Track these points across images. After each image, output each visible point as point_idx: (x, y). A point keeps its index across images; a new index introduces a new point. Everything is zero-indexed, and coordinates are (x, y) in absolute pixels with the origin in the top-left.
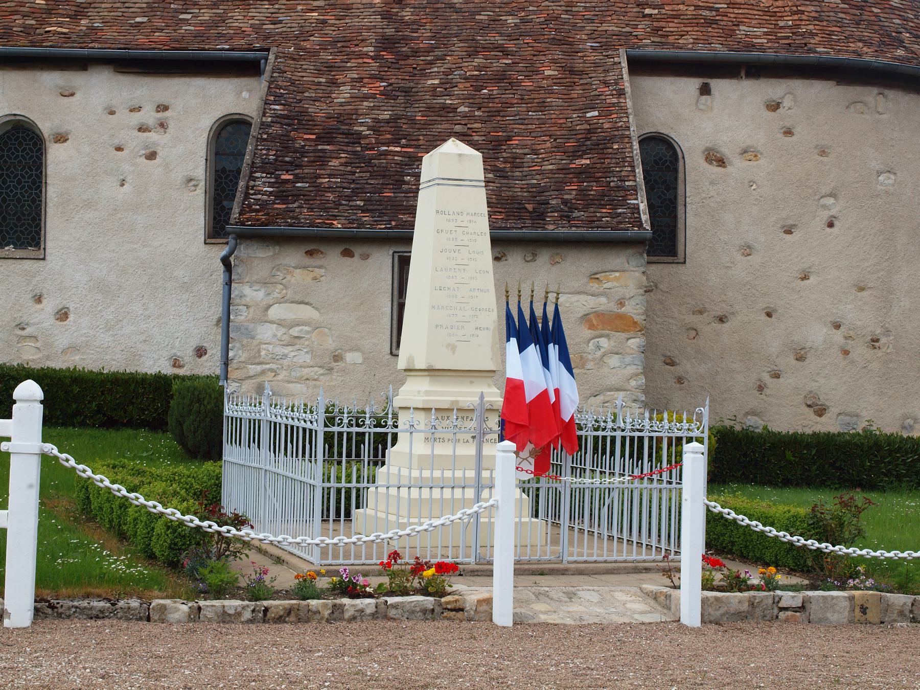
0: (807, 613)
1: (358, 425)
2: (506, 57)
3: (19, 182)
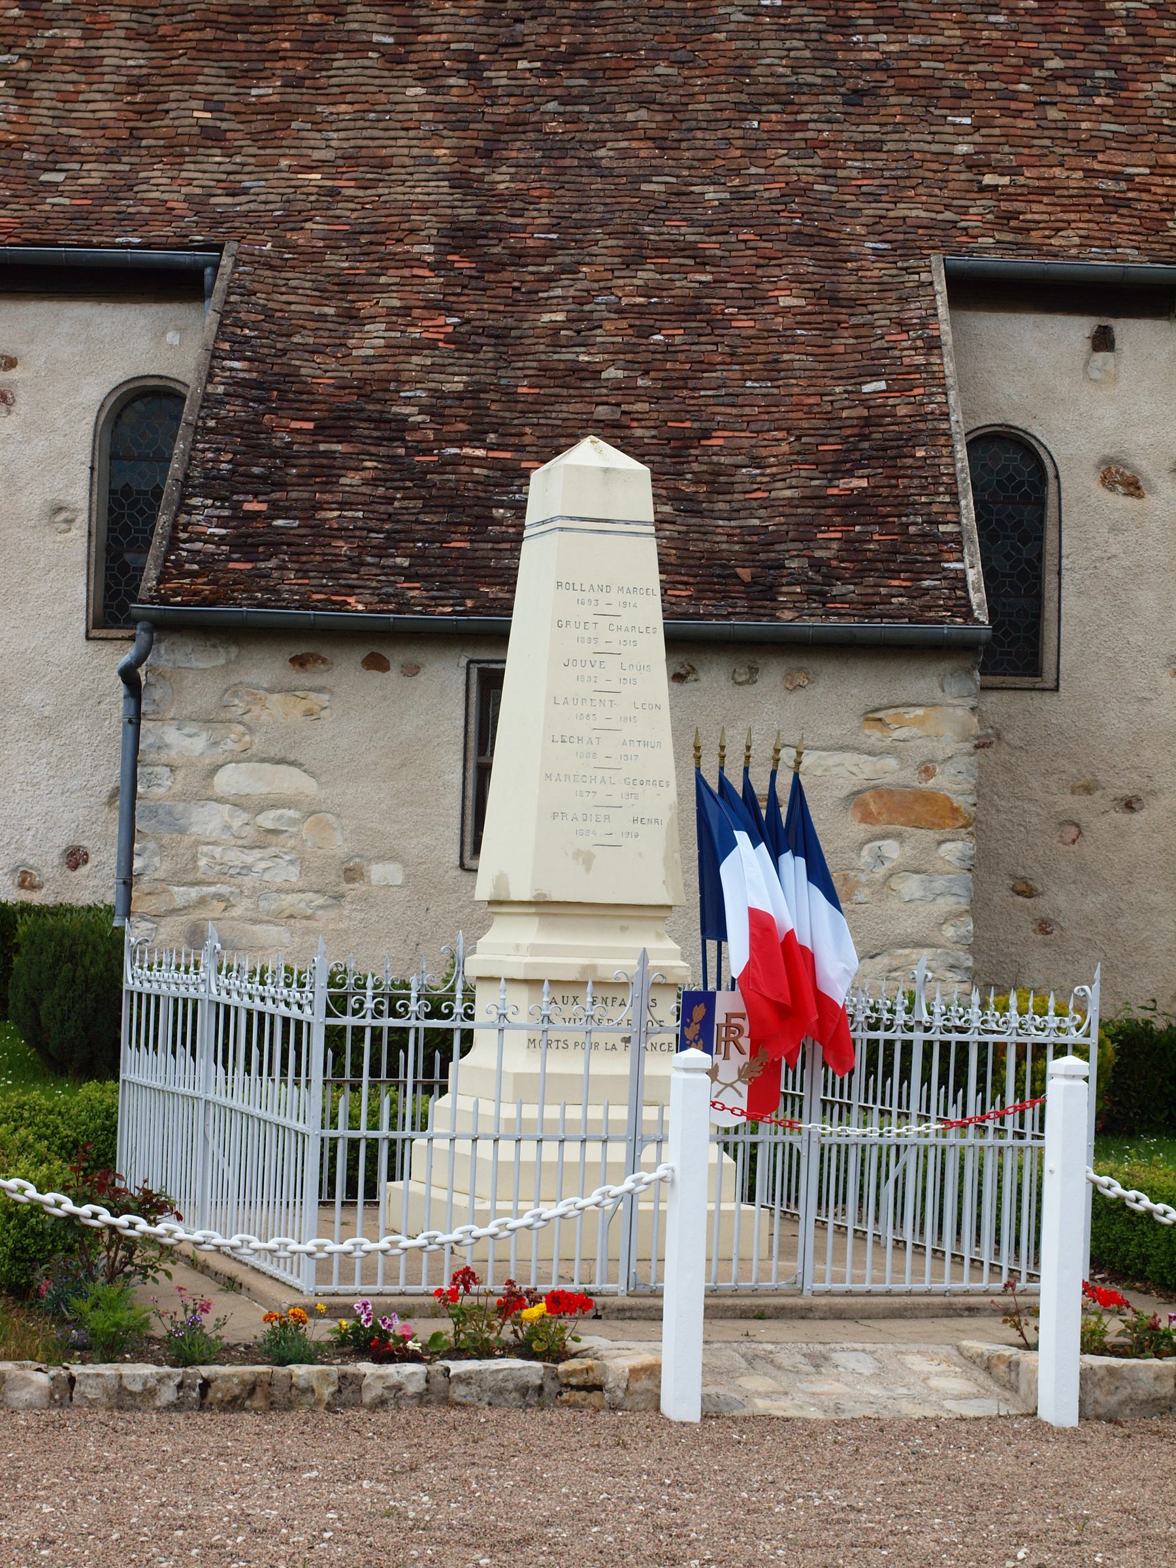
1: (393, 1013)
2: (701, 268)
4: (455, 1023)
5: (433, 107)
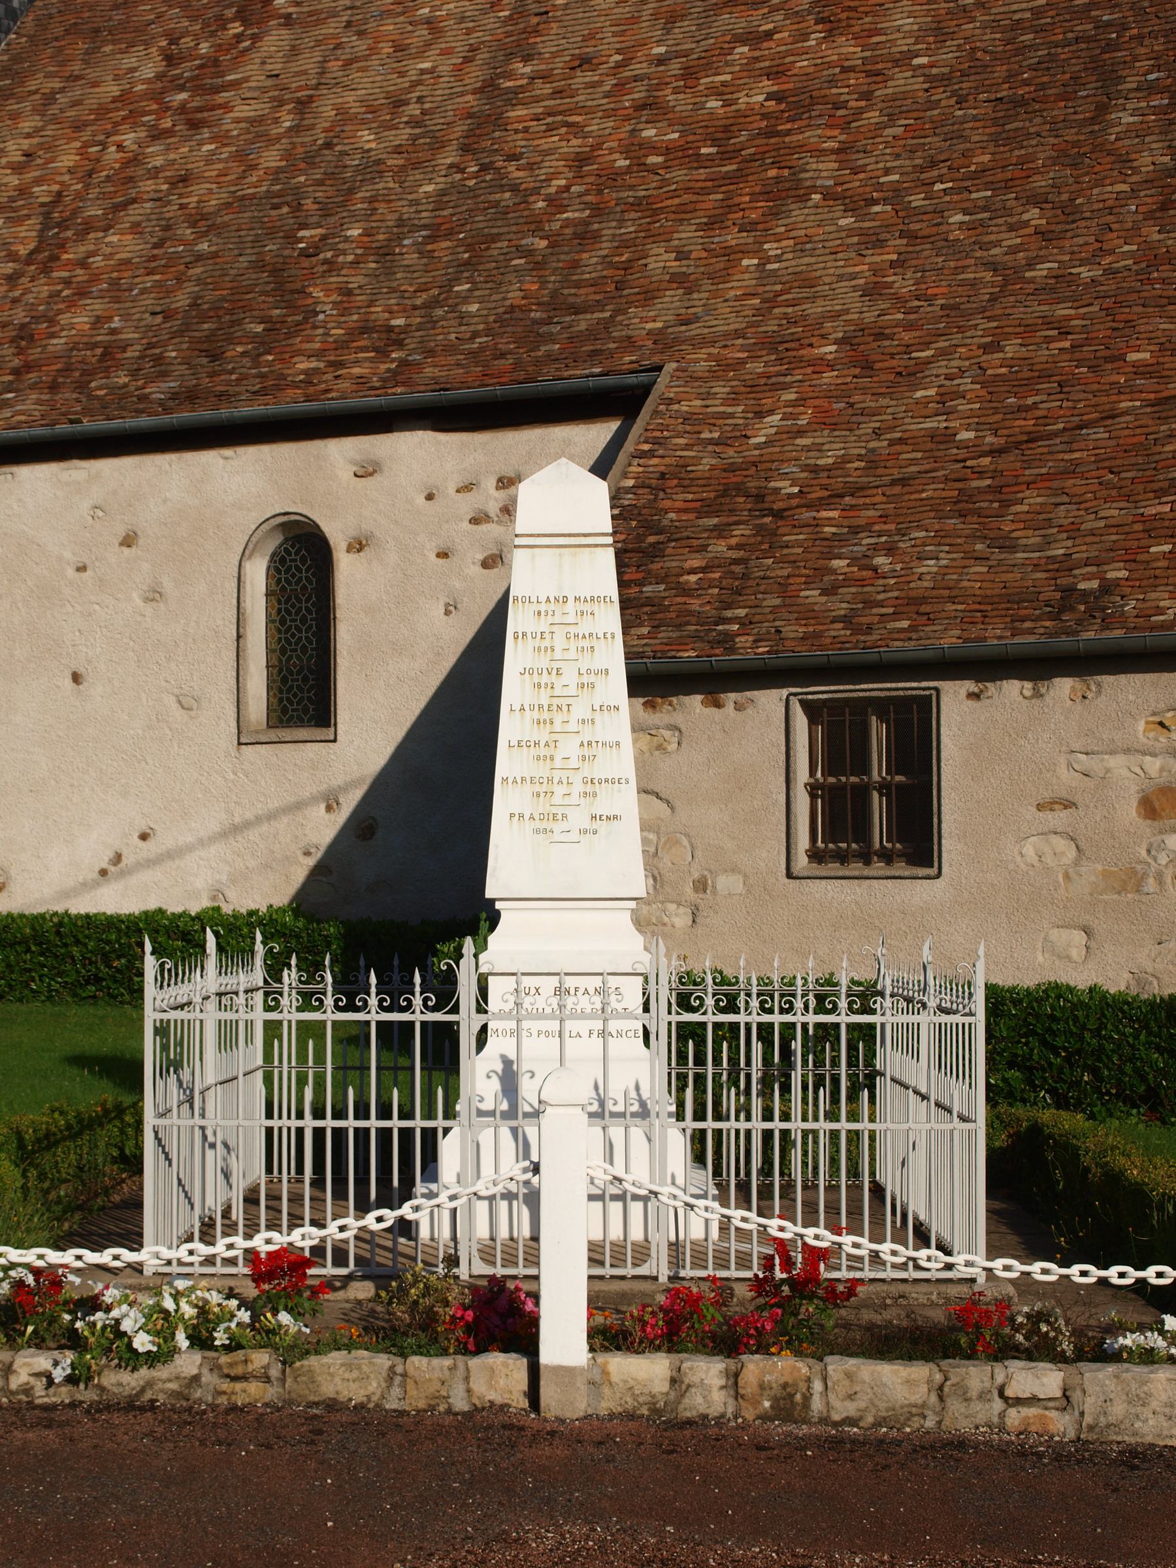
0: (1077, 1413)
1: (820, 1009)
2: (1064, 336)
3: (304, 620)
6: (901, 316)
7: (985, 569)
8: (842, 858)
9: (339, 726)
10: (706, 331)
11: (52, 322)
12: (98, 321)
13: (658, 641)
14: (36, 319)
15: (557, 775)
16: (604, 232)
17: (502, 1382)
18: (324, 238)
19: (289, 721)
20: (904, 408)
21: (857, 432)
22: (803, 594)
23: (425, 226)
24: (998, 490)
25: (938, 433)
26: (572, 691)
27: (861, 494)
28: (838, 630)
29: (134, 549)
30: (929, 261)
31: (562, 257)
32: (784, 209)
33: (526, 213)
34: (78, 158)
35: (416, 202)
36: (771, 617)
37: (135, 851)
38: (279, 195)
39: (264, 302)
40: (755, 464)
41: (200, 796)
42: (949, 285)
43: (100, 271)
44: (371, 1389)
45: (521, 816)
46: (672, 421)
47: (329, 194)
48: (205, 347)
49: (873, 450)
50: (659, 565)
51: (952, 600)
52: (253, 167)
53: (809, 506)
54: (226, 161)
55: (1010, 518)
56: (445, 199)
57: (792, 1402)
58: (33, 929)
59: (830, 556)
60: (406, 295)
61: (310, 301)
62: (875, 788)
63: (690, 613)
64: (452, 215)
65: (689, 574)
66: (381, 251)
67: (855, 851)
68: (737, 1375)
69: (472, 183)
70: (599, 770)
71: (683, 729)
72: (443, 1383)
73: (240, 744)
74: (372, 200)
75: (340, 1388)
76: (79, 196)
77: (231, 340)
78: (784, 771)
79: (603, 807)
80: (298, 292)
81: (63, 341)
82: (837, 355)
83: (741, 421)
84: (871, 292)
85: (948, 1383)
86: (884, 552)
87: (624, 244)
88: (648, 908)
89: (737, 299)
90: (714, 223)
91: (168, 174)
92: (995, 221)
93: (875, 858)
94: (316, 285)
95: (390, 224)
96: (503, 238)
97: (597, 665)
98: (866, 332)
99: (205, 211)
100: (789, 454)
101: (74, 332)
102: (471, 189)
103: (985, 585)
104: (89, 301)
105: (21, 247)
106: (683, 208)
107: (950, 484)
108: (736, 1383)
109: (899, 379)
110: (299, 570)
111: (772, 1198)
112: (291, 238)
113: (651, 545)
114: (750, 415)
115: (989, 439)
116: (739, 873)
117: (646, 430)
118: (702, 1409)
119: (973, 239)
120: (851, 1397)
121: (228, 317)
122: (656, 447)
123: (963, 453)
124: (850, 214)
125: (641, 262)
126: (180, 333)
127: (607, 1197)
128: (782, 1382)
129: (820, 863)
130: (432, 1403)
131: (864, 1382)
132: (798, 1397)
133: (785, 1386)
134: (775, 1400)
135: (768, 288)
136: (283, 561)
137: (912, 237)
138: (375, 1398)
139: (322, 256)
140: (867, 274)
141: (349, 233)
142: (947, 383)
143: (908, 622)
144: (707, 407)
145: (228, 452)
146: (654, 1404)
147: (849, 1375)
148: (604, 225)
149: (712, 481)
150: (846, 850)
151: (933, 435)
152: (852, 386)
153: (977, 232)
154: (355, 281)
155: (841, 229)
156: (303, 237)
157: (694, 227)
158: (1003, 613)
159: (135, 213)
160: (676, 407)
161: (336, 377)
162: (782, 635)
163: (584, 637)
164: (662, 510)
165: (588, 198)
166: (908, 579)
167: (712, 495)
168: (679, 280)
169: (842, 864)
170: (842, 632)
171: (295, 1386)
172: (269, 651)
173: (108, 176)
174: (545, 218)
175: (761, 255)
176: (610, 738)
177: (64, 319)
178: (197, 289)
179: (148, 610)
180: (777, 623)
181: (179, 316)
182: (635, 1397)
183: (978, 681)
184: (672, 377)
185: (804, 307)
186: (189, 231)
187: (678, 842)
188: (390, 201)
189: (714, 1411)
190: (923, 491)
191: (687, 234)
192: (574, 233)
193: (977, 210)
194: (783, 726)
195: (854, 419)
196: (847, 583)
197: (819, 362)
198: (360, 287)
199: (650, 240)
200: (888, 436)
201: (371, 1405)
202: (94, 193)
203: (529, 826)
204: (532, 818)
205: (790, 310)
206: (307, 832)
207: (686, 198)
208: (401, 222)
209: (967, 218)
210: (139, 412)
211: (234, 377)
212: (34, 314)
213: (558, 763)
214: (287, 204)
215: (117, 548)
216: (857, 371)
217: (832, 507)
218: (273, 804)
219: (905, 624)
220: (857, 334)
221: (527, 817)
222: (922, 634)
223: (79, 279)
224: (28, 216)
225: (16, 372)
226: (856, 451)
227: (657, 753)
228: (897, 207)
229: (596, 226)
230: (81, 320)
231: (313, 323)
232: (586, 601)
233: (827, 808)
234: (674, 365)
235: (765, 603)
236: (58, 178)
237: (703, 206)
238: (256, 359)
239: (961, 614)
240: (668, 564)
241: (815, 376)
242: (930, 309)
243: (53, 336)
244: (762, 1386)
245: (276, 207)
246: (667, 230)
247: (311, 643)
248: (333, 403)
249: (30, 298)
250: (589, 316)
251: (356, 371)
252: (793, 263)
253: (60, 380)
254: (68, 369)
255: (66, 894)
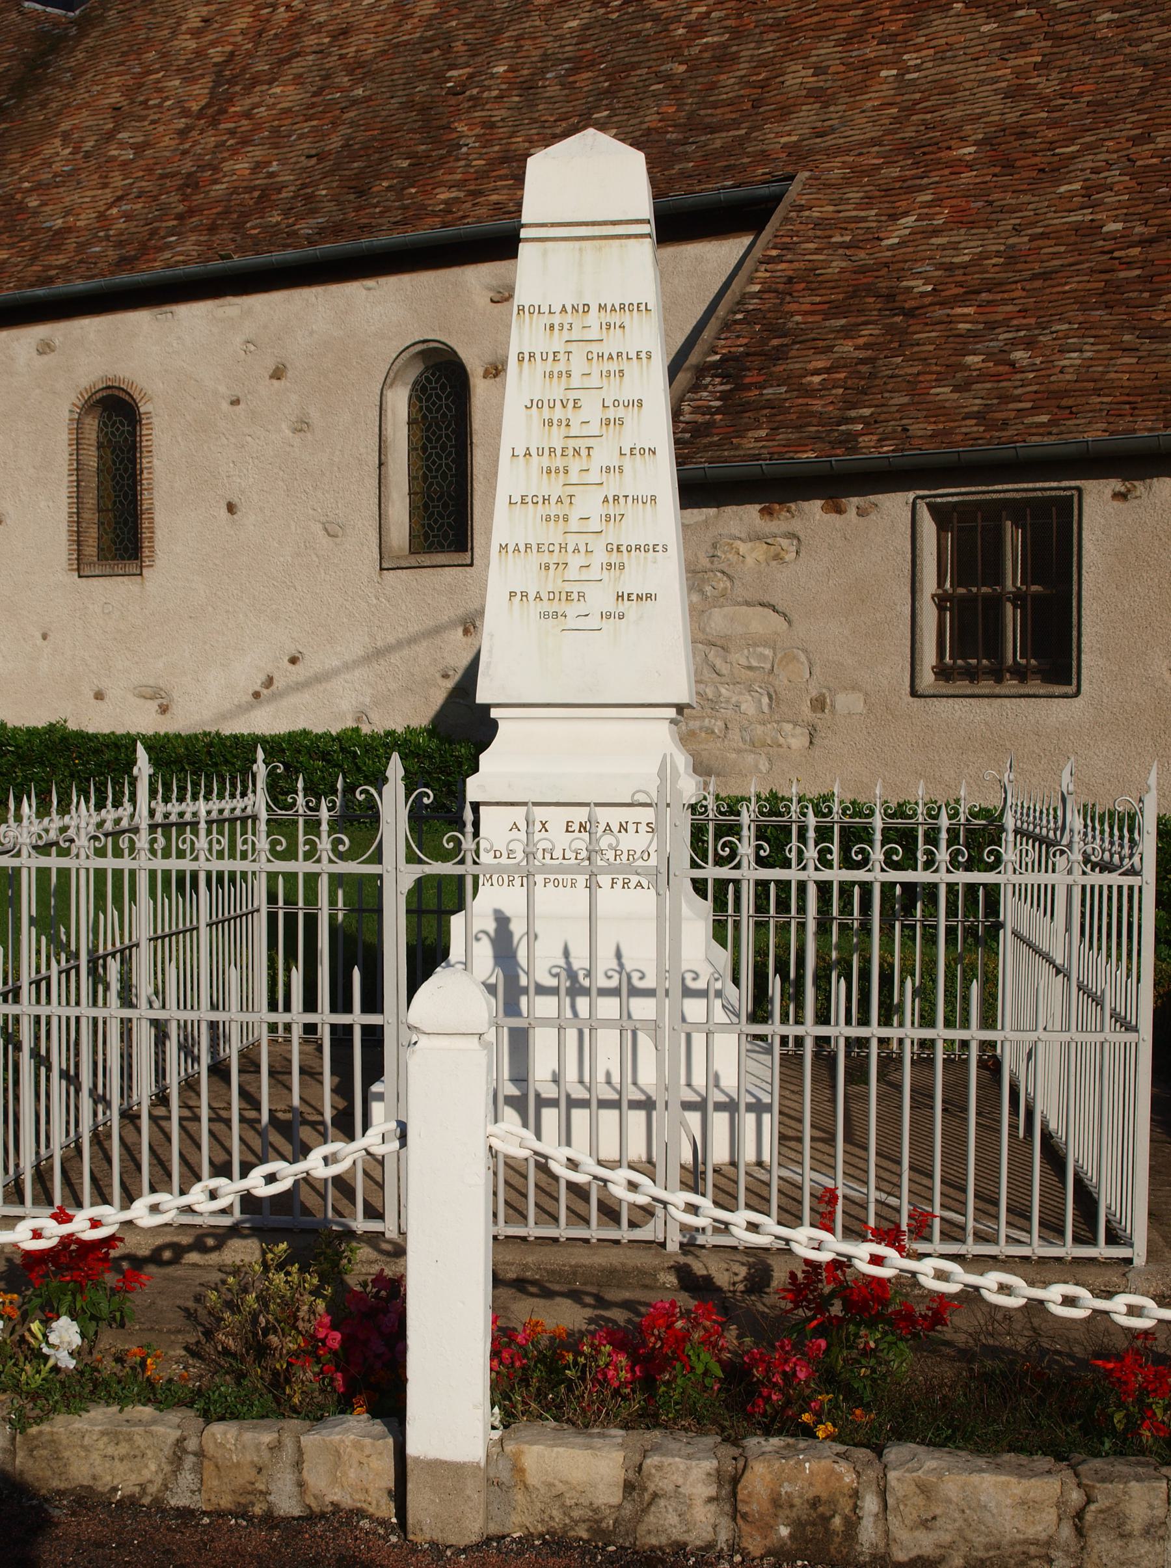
3: (443, 448)
4: (468, 869)
5: (1002, 37)
6: (1045, 115)
7: (1134, 360)
8: (972, 675)
9: (475, 550)
10: (842, 141)
11: (216, 169)
12: (258, 166)
13: (776, 443)
14: (201, 168)
15: (572, 541)
16: (742, 54)
17: (352, 1474)
18: (471, 76)
19: (430, 547)
20: (1046, 203)
21: (995, 230)
22: (933, 391)
23: (567, 59)
24: (1150, 279)
25: (1083, 226)
26: (594, 429)
27: (999, 289)
28: (971, 427)
29: (283, 382)
30: (1075, 60)
31: (700, 80)
32: (924, 19)
33: (666, 41)
34: (250, 20)
35: (561, 38)
36: (898, 416)
37: (286, 675)
38: (431, 40)
39: (411, 139)
40: (886, 265)
41: (345, 620)
42: (1097, 83)
43: (263, 120)
44: (147, 1474)
45: (524, 595)
46: (803, 227)
47: (478, 36)
48: (353, 184)
49: (1013, 246)
50: (781, 368)
51: (1097, 392)
52: (410, 16)
53: (942, 304)
54: (384, 12)
55: (1163, 307)
56: (588, 33)
57: (827, 1530)
58: (187, 749)
59: (963, 352)
60: (547, 125)
61: (455, 135)
62: (1008, 599)
63: (812, 414)
64: (595, 47)
65: (812, 375)
66: (525, 86)
67: (986, 667)
68: (735, 1480)
69: (614, 16)
70: (629, 534)
71: (802, 537)
72: (260, 1470)
73: (381, 569)
74: (518, 38)
75: (98, 1470)
76: (249, 55)
77: (379, 177)
78: (909, 581)
79: (632, 583)
80: (444, 128)
81: (224, 186)
82: (976, 155)
83: (874, 224)
84: (1014, 94)
85: (1093, 1507)
86: (1022, 346)
87: (762, 64)
88: (763, 728)
89: (874, 109)
90: (854, 37)
91: (331, 28)
92: (1145, 17)
93: (1008, 676)
94: (461, 120)
95: (534, 59)
96: (643, 65)
97: (627, 395)
98: (1007, 132)
99: (362, 59)
100: (923, 254)
101: (235, 177)
102: (614, 22)
103: (1134, 376)
104: (251, 149)
105: (194, 104)
106: (822, 25)
107: (1095, 276)
108: (734, 1494)
109: (1042, 175)
110: (439, 398)
111: (866, 1082)
112: (441, 78)
113: (774, 347)
114: (883, 218)
115: (1139, 229)
116: (860, 690)
117: (776, 236)
118: (677, 1534)
119: (1122, 36)
120: (926, 1524)
121: (377, 155)
122: (784, 252)
123: (1109, 245)
124: (993, 20)
125: (778, 80)
126: (331, 173)
127: (625, 1105)
128: (810, 1495)
129: (947, 680)
130: (243, 1500)
131: (949, 1501)
132: (837, 1521)
133: (815, 1502)
134: (798, 1526)
135: (906, 97)
136: (424, 389)
137: (1057, 38)
138: (152, 1489)
139: (468, 93)
140: (1009, 77)
141: (495, 70)
142: (1094, 176)
143: (1049, 417)
144: (840, 212)
145: (370, 283)
146: (597, 1522)
147: (924, 1489)
148: (742, 47)
149: (842, 284)
150: (976, 667)
151: (1077, 228)
152: (992, 185)
153: (1127, 28)
154: (499, 114)
155: (983, 35)
156: (452, 77)
157: (833, 43)
158: (1155, 404)
159: (298, 65)
160: (807, 213)
161: (474, 205)
162: (909, 434)
163: (611, 357)
164: (787, 313)
165: (728, 23)
166: (1049, 372)
167: (841, 297)
168: (817, 95)
169: (971, 681)
170: (975, 429)
171: (30, 1463)
172: (412, 479)
173: (276, 34)
174: (685, 43)
175: (900, 65)
176: (644, 491)
177: (227, 167)
178: (349, 131)
179: (296, 440)
180: (904, 422)
181: (331, 157)
182: (566, 1510)
183: (1125, 479)
184: (805, 185)
185: (943, 112)
186: (346, 79)
187: (795, 658)
188: (536, 38)
189: (698, 1536)
190: (1066, 284)
191: (826, 50)
192: (713, 57)
193: (1126, 7)
194: (909, 531)
195: (993, 216)
196: (982, 379)
197: (958, 163)
198: (503, 120)
199: (788, 58)
200: (1029, 232)
201: (146, 1501)
202: (262, 50)
203: (535, 608)
204: (538, 597)
205: (929, 116)
206: (445, 655)
207: (825, 16)
208: (545, 57)
209: (1116, 16)
210: (286, 246)
211: (378, 210)
212: (200, 163)
213: (574, 525)
214: (438, 47)
215: (267, 381)
216: (997, 170)
217: (968, 303)
218: (414, 628)
219: (1044, 418)
220: (998, 134)
221: (532, 596)
222: (1063, 428)
223: (243, 129)
224: (202, 76)
225: (180, 217)
226: (994, 248)
227: (775, 563)
228: (1042, 10)
229: (734, 49)
230: (242, 166)
231: (456, 156)
232: (613, 309)
233: (956, 620)
234: (807, 174)
235: (892, 402)
236: (232, 40)
237: (843, 22)
238: (400, 191)
239: (1108, 407)
240: (791, 366)
241: (953, 177)
242: (1075, 106)
243: (216, 182)
244: (776, 1502)
245: (427, 51)
246: (805, 48)
247: (450, 469)
248: (468, 227)
249: (198, 149)
250: (724, 134)
251: (494, 198)
252: (933, 71)
253: (219, 222)
254: (227, 212)
255: (224, 717)
